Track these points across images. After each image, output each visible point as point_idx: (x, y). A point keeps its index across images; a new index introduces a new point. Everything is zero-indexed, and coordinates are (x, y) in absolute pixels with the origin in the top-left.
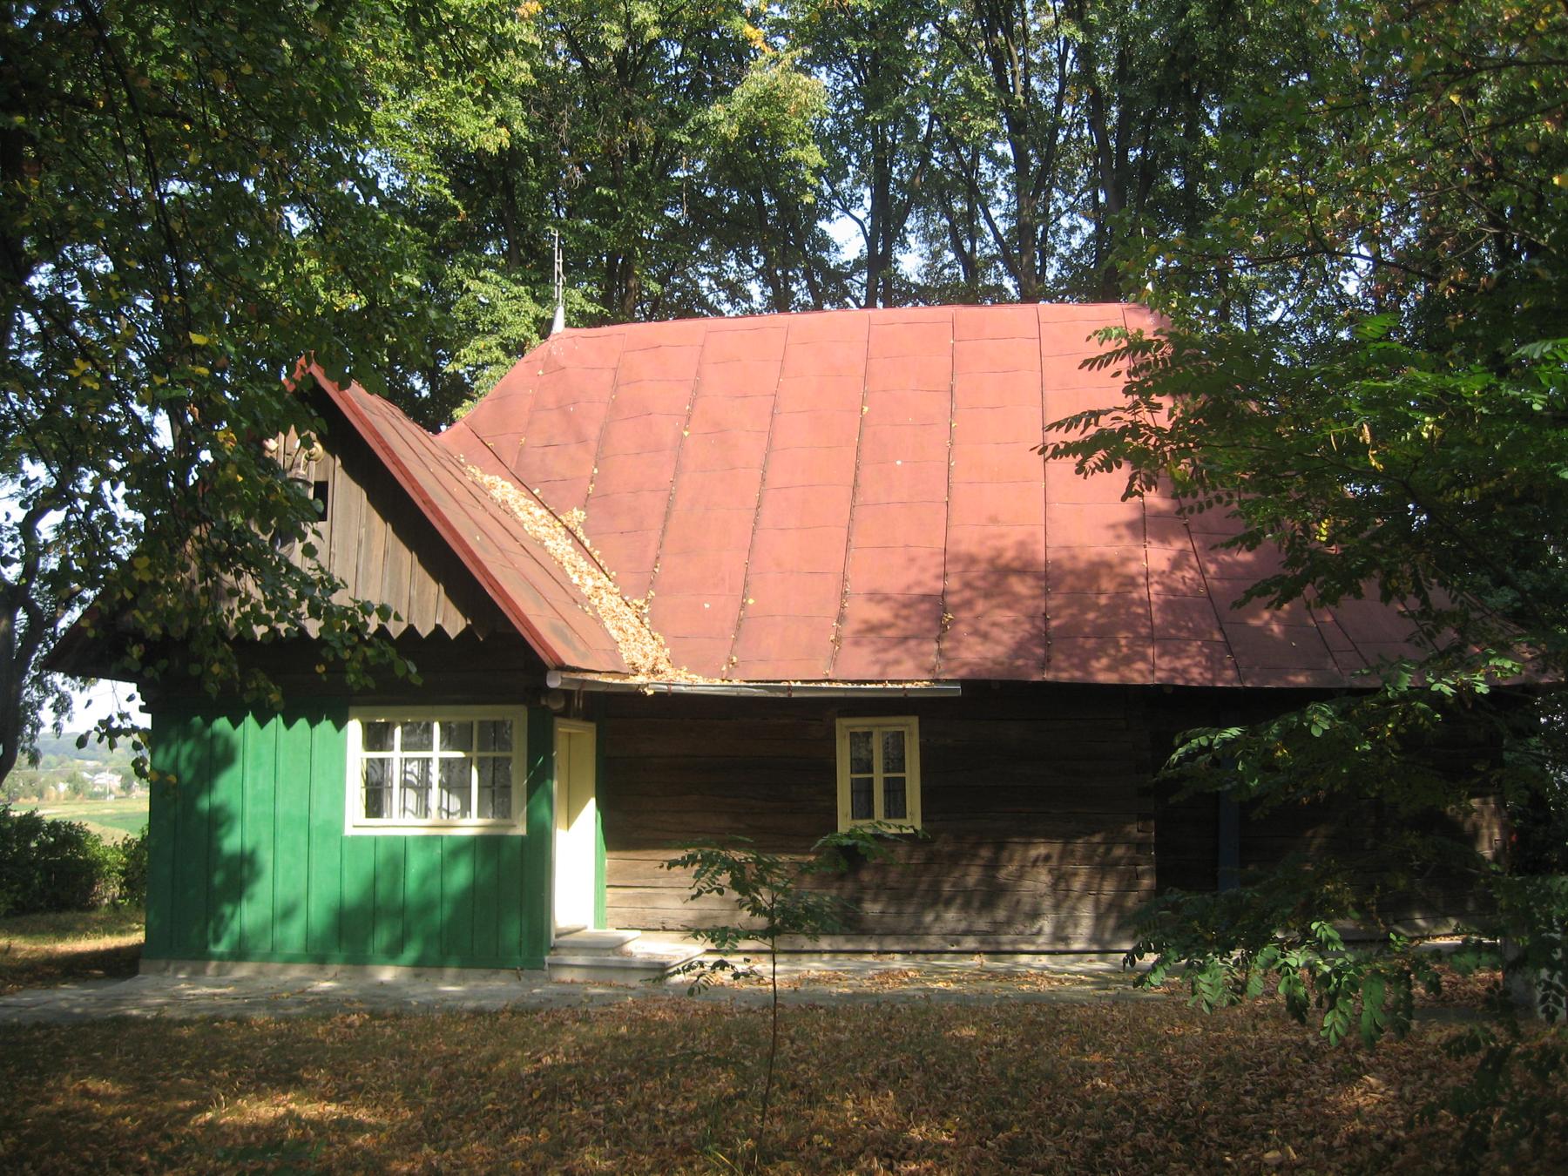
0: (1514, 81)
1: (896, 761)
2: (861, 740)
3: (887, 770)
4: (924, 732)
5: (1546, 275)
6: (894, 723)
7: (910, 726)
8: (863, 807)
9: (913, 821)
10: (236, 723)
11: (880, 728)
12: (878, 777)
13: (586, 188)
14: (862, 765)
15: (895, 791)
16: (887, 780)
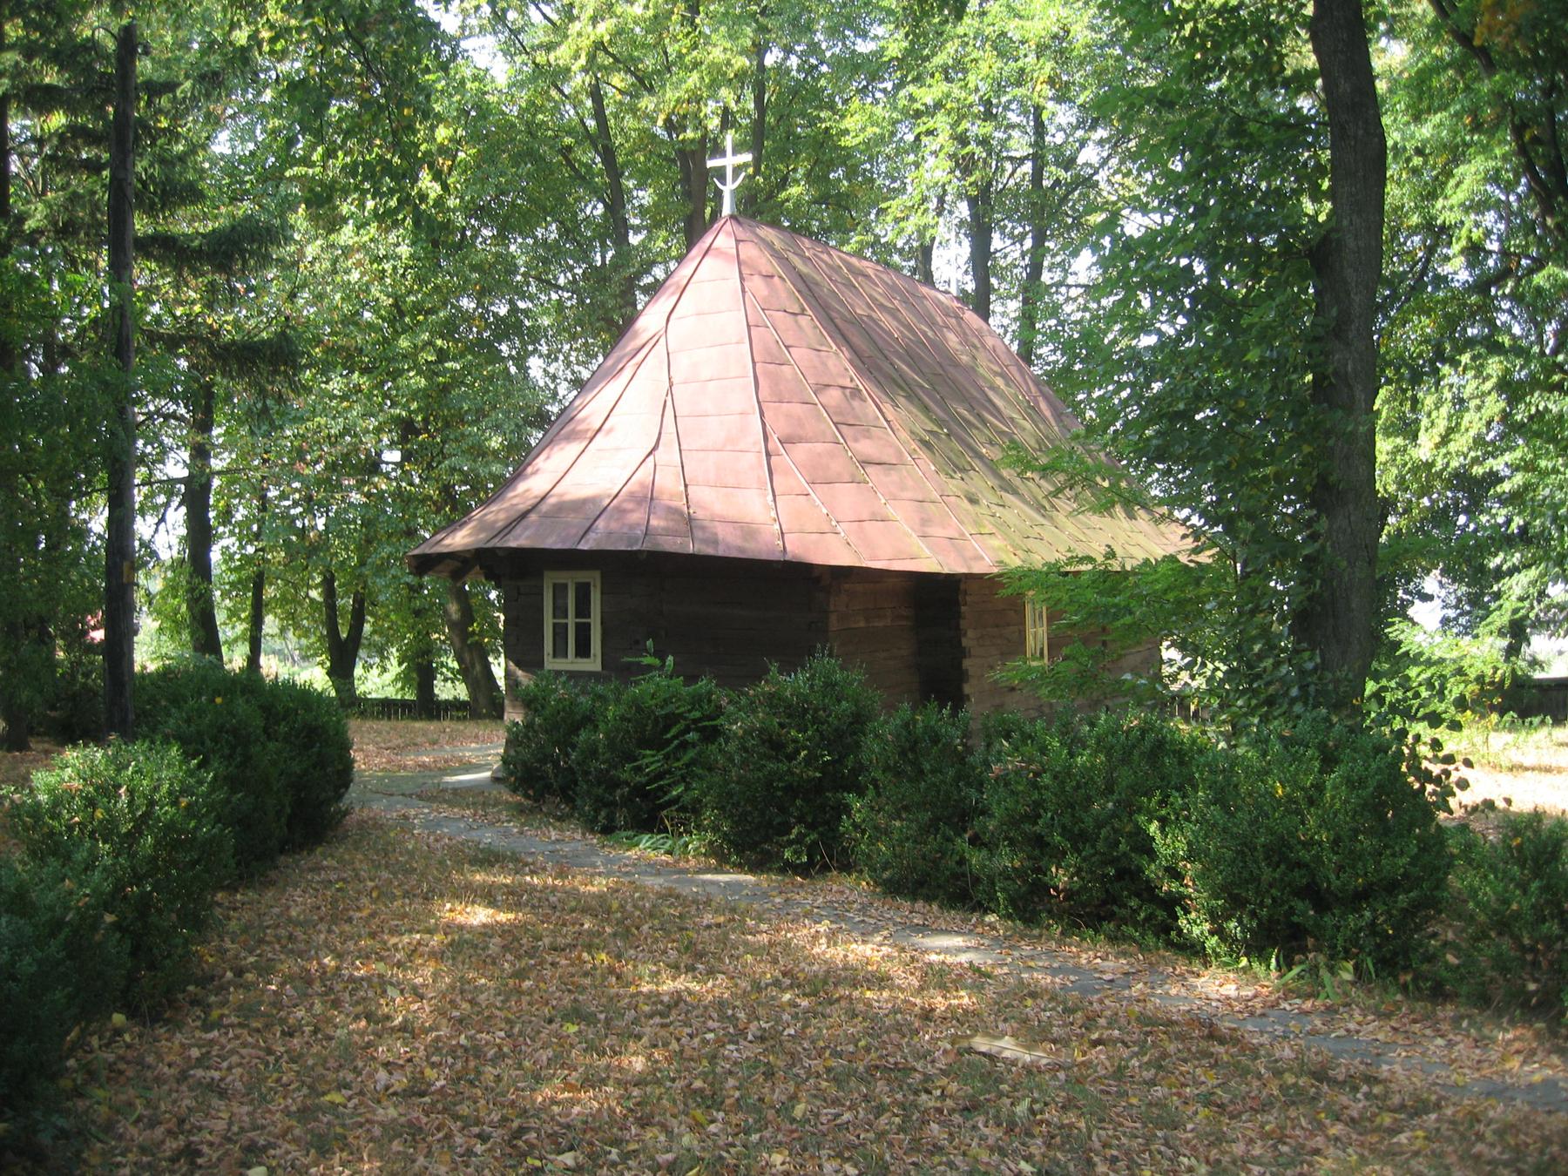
0: (81, 547)
1: (583, 609)
2: (560, 590)
3: (577, 616)
4: (602, 577)
5: (119, 1159)
6: (583, 576)
7: (594, 578)
8: (560, 651)
9: (593, 664)
10: (324, 690)
11: (571, 579)
12: (571, 621)
13: (621, 240)
14: (560, 611)
15: (583, 634)
16: (577, 624)
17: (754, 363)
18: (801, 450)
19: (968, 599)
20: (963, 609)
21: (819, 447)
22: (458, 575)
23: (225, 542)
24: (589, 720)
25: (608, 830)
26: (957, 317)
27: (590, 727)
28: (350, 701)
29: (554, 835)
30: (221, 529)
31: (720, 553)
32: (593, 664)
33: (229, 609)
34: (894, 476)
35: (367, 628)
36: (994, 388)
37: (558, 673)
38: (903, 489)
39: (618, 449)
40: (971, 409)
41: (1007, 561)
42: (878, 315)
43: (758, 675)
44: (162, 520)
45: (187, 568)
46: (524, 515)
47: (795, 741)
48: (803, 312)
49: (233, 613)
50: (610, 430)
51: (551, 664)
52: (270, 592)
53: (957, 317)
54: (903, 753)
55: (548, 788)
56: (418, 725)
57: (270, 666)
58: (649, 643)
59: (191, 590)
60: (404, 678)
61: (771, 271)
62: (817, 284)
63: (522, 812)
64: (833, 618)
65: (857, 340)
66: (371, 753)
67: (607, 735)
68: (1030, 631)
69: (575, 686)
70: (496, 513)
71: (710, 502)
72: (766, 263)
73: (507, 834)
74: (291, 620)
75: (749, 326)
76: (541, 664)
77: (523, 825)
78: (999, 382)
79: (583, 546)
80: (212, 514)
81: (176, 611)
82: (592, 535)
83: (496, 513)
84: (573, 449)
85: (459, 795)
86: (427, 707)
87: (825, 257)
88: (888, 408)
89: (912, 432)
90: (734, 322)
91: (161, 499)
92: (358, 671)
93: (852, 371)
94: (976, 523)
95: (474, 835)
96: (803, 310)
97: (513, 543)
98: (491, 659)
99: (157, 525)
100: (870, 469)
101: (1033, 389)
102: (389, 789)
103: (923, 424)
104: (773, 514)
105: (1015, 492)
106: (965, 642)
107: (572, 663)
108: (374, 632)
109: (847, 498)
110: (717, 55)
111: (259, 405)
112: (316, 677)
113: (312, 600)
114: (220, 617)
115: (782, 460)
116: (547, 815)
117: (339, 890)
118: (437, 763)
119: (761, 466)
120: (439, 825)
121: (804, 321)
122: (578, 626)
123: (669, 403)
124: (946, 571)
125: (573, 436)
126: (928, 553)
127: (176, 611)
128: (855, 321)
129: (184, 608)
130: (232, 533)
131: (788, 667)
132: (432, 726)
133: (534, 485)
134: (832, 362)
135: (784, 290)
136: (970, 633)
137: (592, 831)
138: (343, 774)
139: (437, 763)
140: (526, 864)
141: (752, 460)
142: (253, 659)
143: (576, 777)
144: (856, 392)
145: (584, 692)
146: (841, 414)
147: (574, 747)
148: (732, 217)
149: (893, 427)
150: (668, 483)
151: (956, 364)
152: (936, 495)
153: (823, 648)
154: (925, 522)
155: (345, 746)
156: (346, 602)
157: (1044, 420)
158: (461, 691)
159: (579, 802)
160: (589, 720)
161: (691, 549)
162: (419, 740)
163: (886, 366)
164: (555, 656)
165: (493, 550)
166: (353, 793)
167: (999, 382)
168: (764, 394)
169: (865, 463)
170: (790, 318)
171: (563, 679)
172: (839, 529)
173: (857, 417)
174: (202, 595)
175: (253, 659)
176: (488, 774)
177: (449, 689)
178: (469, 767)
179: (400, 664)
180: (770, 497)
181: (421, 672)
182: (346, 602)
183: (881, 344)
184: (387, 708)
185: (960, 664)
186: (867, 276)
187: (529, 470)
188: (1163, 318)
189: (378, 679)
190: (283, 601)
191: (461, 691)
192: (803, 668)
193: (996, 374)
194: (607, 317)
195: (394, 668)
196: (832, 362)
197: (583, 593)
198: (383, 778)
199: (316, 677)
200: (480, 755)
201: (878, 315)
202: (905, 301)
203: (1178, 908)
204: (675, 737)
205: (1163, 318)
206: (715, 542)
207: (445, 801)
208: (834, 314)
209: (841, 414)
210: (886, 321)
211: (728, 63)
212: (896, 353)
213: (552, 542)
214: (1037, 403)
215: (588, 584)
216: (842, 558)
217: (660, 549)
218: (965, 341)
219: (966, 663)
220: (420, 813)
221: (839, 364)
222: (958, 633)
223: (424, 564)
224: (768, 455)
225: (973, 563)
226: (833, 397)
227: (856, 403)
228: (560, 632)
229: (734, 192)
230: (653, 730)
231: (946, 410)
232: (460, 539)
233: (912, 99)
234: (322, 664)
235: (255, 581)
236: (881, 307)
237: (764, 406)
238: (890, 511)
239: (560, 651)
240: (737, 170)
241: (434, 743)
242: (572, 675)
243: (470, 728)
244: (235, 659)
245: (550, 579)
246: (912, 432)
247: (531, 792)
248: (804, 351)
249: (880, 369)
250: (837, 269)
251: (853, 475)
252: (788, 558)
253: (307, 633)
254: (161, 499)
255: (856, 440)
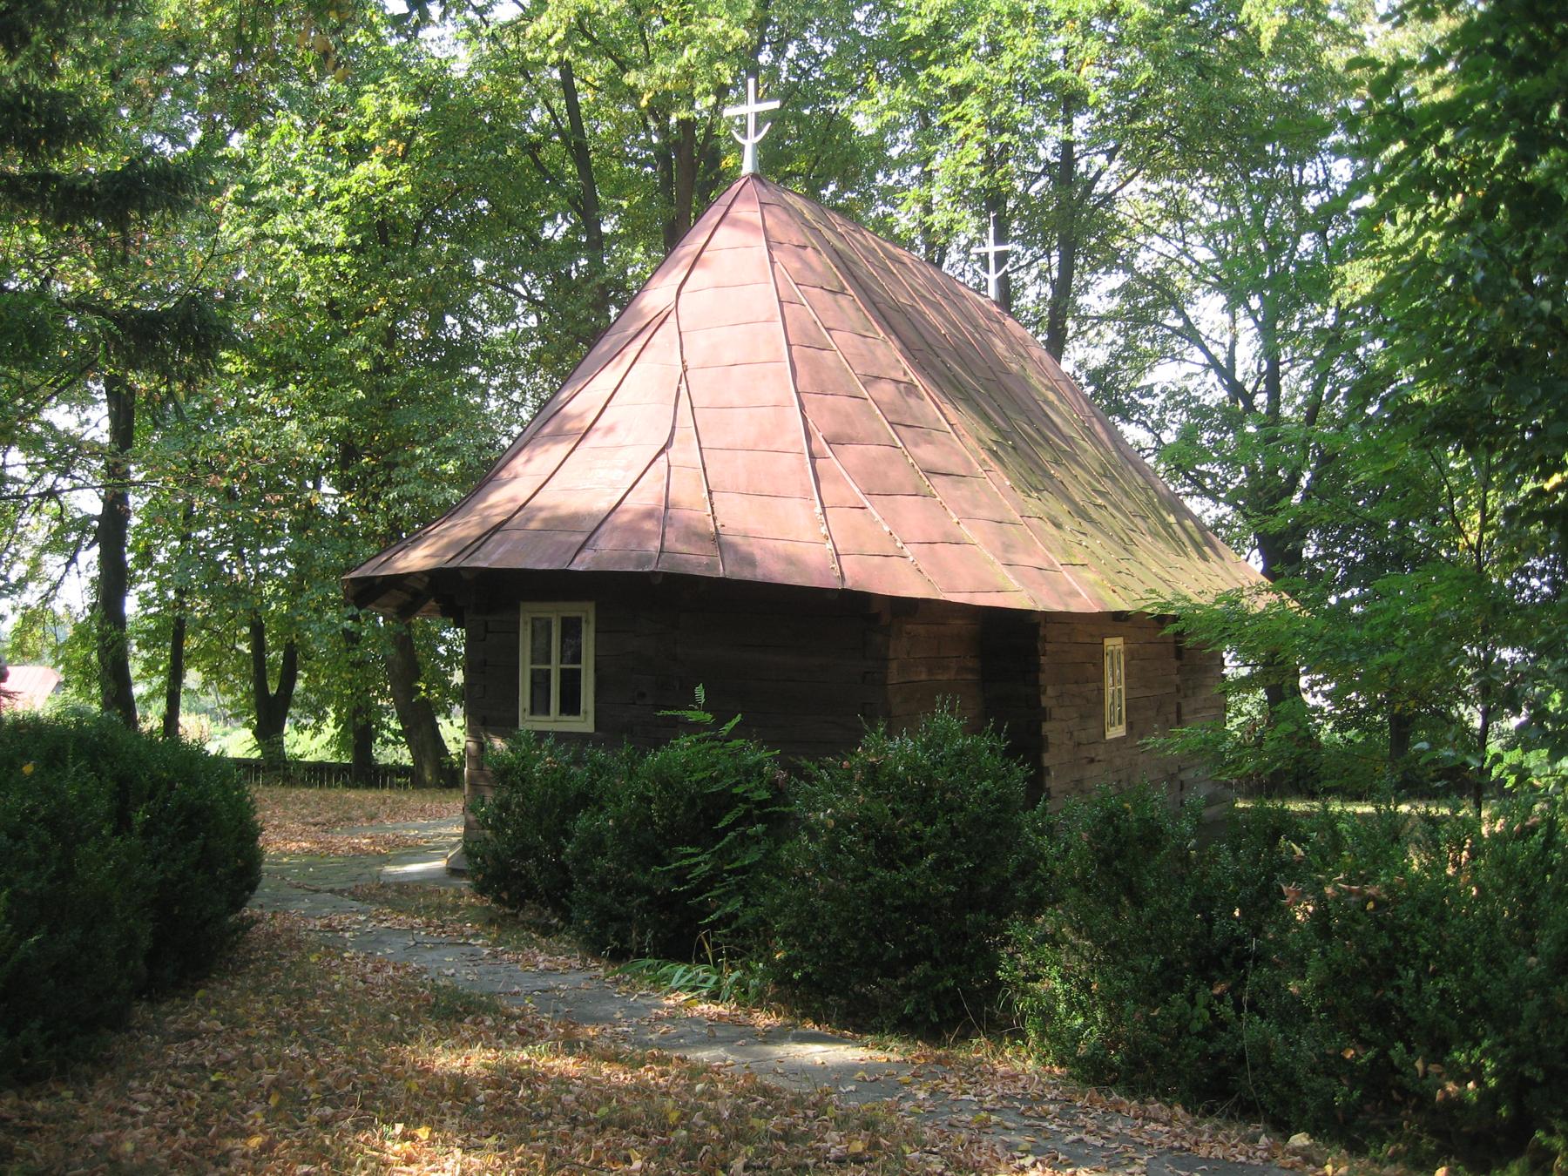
2: (541, 629)
6: (572, 609)
7: (586, 612)
8: (540, 705)
9: (584, 723)
11: (555, 612)
12: (555, 668)
14: (541, 655)
15: (571, 682)
17: (789, 345)
18: (852, 452)
19: (1049, 647)
20: (1043, 659)
21: (873, 450)
22: (405, 612)
23: (143, 587)
24: (585, 800)
25: (619, 956)
26: (999, 322)
28: (275, 765)
29: (542, 960)
30: (139, 572)
31: (760, 578)
32: (584, 723)
33: (146, 661)
34: (962, 492)
35: (300, 685)
36: (1046, 401)
37: (541, 735)
38: (977, 506)
39: (620, 447)
40: (1031, 423)
41: (1107, 599)
42: (922, 306)
43: (852, 742)
44: (73, 559)
46: (497, 528)
47: (915, 836)
48: (843, 291)
49: (150, 666)
50: (611, 429)
51: (528, 723)
52: (191, 643)
53: (999, 322)
54: (1106, 861)
55: (530, 892)
56: (352, 795)
57: (191, 725)
58: (700, 692)
59: (102, 638)
60: (341, 742)
61: (803, 241)
62: (855, 263)
63: (491, 922)
64: (894, 666)
65: (904, 328)
66: (287, 835)
67: (618, 820)
69: (566, 752)
70: (463, 528)
71: (739, 516)
72: (792, 235)
73: (474, 958)
74: (215, 673)
75: (780, 301)
76: (515, 722)
77: (496, 942)
78: (1051, 396)
79: (578, 566)
80: (129, 557)
81: (86, 661)
83: (463, 528)
84: (561, 449)
85: (406, 894)
86: (361, 771)
87: (858, 236)
88: (948, 409)
89: (980, 440)
90: (762, 298)
91: (73, 537)
92: (288, 728)
93: (904, 364)
94: (1066, 551)
95: (426, 959)
96: (844, 288)
97: (481, 561)
98: (439, 720)
99: (68, 565)
100: (936, 480)
101: (1086, 409)
102: (315, 880)
103: (989, 436)
104: (824, 530)
105: (1091, 520)
106: (1045, 701)
107: (555, 722)
108: (307, 689)
109: (912, 515)
110: (716, 26)
111: (163, 389)
112: (238, 742)
113: (240, 652)
114: (135, 668)
115: (831, 464)
116: (528, 926)
117: (215, 1087)
118: (374, 851)
119: (806, 472)
120: (379, 941)
121: (844, 301)
123: (684, 391)
124: (1040, 608)
125: (558, 436)
126: (1016, 585)
127: (86, 661)
128: (900, 309)
129: (94, 657)
130: (151, 578)
132: (370, 795)
133: (499, 500)
134: (880, 351)
135: (820, 262)
136: (1050, 691)
137: (596, 955)
138: (244, 869)
139: (374, 851)
140: (511, 1018)
141: (793, 464)
142: (171, 719)
143: (587, 879)
144: (911, 388)
145: (577, 761)
146: (896, 412)
147: (569, 838)
148: (754, 176)
149: (958, 437)
150: (688, 493)
151: (1008, 373)
152: (1016, 516)
153: (943, 703)
154: (1007, 547)
155: (247, 834)
156: (275, 656)
157: (1101, 443)
158: (404, 756)
159: (575, 914)
160: (585, 800)
161: (721, 572)
162: (354, 813)
163: (937, 362)
164: (532, 713)
165: (457, 570)
166: (265, 888)
167: (1051, 396)
168: (803, 382)
169: (931, 472)
170: (828, 297)
171: (549, 742)
172: (906, 551)
173: (915, 418)
174: (114, 643)
175: (171, 719)
176: (440, 864)
177: (394, 753)
178: (416, 852)
179: (336, 727)
180: (818, 509)
181: (359, 735)
182: (275, 656)
183: (931, 341)
184: (319, 773)
185: (1039, 728)
186: (904, 264)
187: (504, 474)
189: (312, 742)
190: (206, 652)
191: (404, 756)
193: (1048, 388)
194: (585, 322)
195: (330, 730)
196: (880, 351)
197: (571, 628)
198: (308, 865)
199: (238, 742)
200: (430, 838)
201: (922, 306)
202: (945, 297)
204: (731, 827)
206: (749, 561)
207: (387, 902)
208: (877, 299)
209: (896, 412)
210: (931, 315)
211: (726, 36)
212: (945, 349)
214: (1092, 423)
215: (579, 619)
216: (915, 589)
217: (682, 570)
218: (1011, 347)
219: (1047, 727)
220: (355, 920)
221: (888, 354)
222: (1038, 690)
223: (367, 593)
224: (812, 457)
225: (1069, 600)
226: (886, 391)
227: (912, 401)
228: (540, 682)
229: (760, 145)
230: (704, 815)
231: (1006, 419)
232: (416, 559)
233: (937, 82)
234: (248, 724)
235: (172, 629)
236: (923, 297)
237: (805, 397)
238: (965, 531)
239: (540, 705)
240: (760, 118)
241: (372, 818)
242: (561, 737)
243: (414, 799)
244: (151, 719)
245: (528, 614)
246: (980, 440)
247: (505, 895)
248: (846, 335)
249: (934, 367)
250: (873, 252)
251: (917, 487)
252: (848, 585)
253: (231, 690)
254: (73, 537)
255: (916, 445)
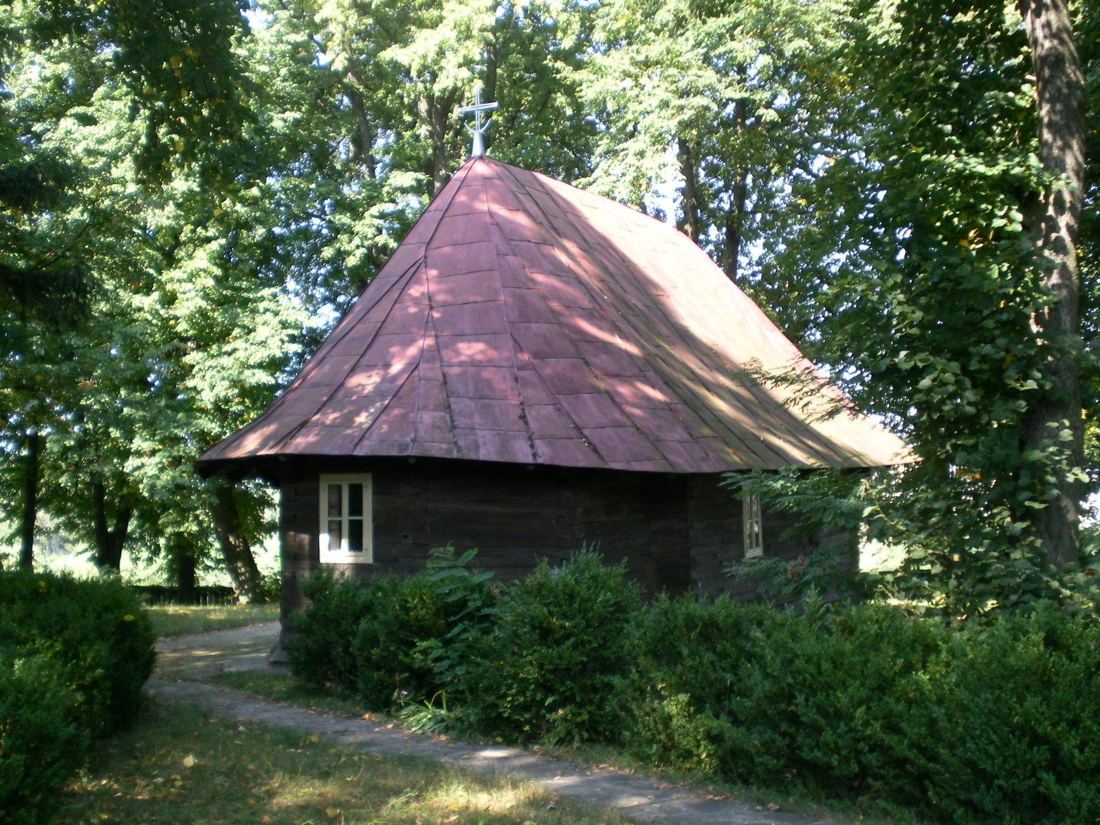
1: (356, 508)
6: (355, 479)
11: (345, 482)
27: (369, 616)
43: (529, 567)
45: (846, 465)
60: (171, 568)
68: (747, 526)
82: (366, 443)
122: (352, 523)
131: (556, 562)
142: (27, 556)
166: (153, 679)
175: (27, 556)
188: (192, 281)
192: (568, 560)
195: (161, 561)
203: (927, 782)
205: (192, 281)
213: (332, 449)
217: (428, 454)
